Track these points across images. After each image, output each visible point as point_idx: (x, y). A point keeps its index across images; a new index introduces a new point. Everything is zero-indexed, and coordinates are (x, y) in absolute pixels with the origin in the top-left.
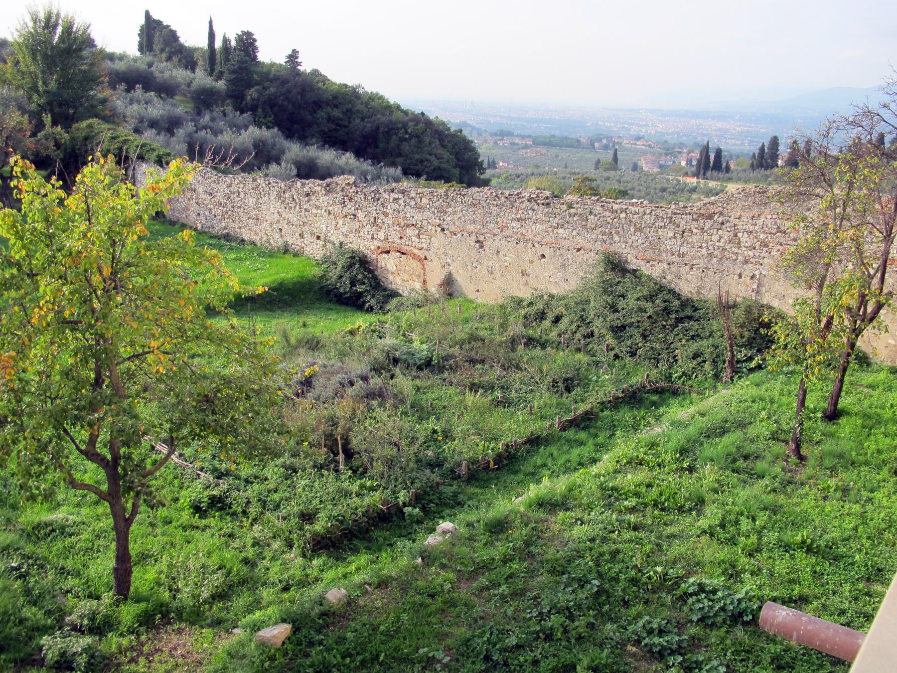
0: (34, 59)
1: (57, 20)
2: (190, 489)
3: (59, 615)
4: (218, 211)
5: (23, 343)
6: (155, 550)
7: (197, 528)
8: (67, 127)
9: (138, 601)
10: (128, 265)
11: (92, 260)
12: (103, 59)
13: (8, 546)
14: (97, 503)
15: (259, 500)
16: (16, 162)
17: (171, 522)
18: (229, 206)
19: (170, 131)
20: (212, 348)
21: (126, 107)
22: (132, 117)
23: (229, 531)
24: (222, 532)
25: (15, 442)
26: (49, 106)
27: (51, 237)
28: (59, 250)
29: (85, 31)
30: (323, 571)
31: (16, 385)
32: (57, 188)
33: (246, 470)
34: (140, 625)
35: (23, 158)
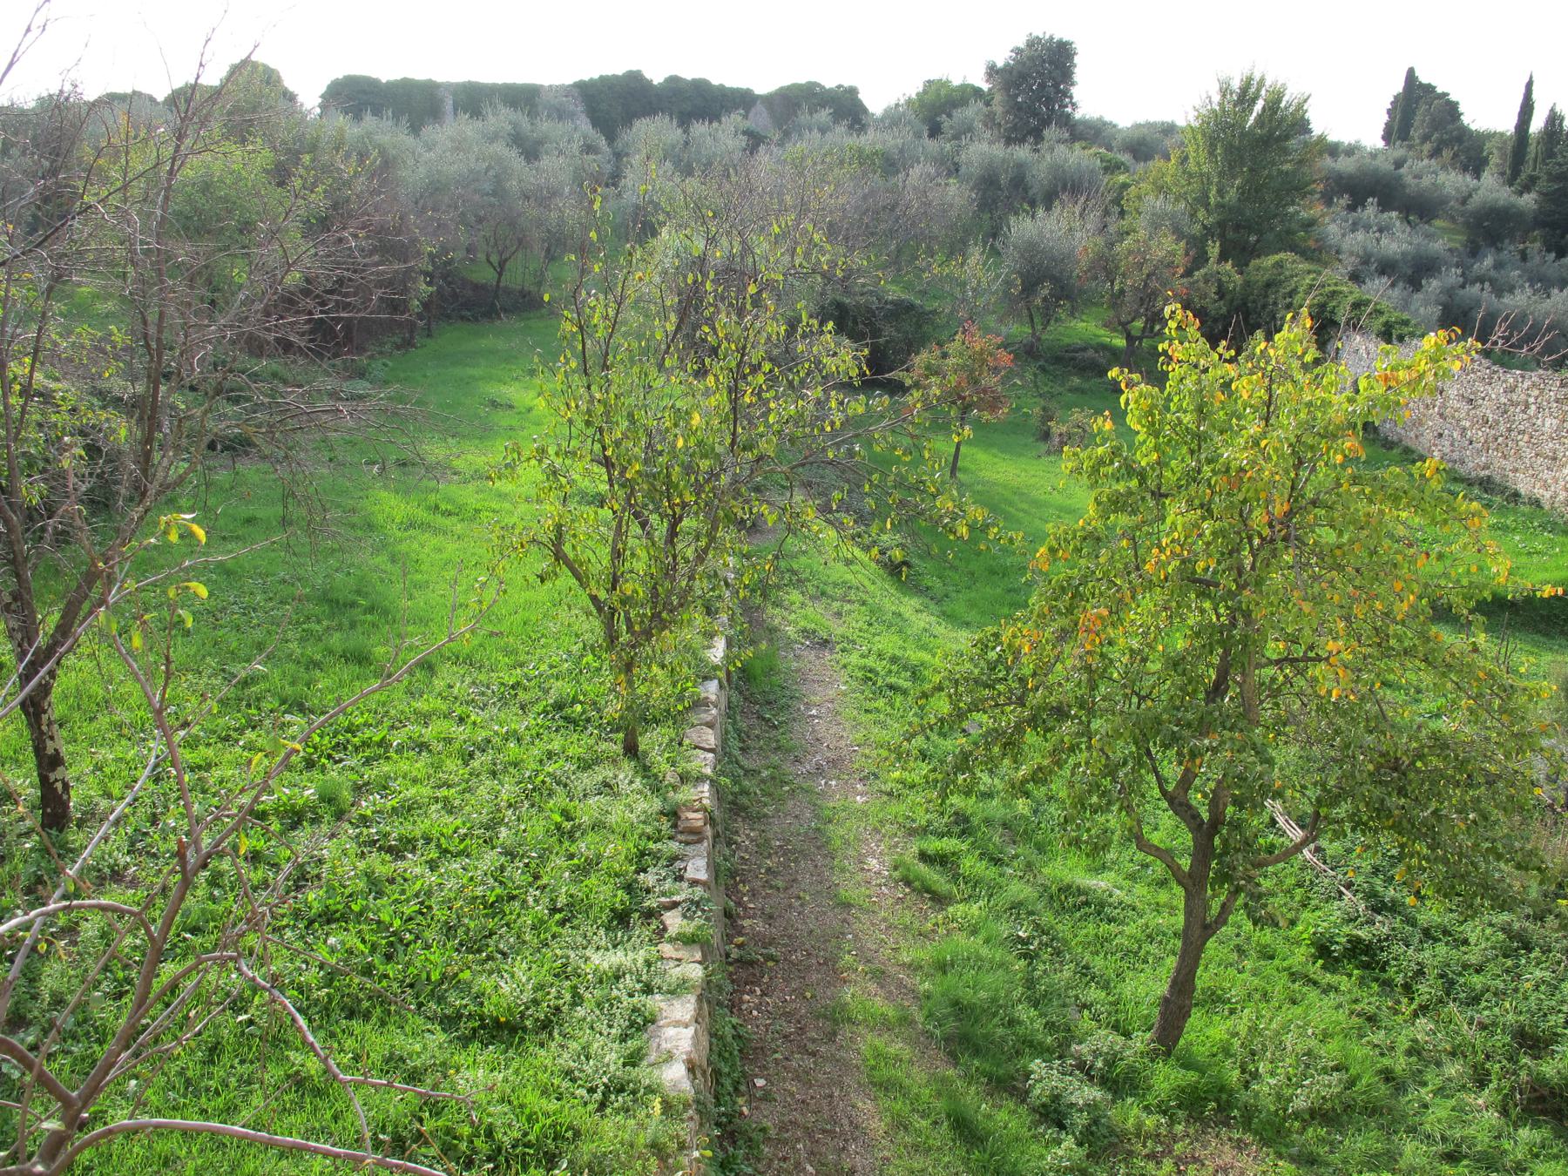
0: (1212, 153)
1: (1258, 90)
2: (1318, 913)
3: (1066, 1036)
4: (1480, 435)
5: (1121, 600)
6: (1235, 993)
7: (1315, 983)
8: (1241, 266)
9: (1187, 1064)
10: (1314, 503)
11: (1260, 485)
12: (1321, 153)
13: (1021, 903)
14: (1162, 883)
15: (1442, 976)
16: (1173, 312)
17: (1272, 958)
18: (1502, 428)
19: (1415, 283)
20: (1428, 678)
21: (1344, 235)
22: (1352, 254)
23: (1372, 1009)
24: (1358, 1007)
25: (1072, 749)
26: (1219, 230)
27: (1201, 438)
28: (1209, 461)
29: (1300, 106)
30: (1537, 1156)
31: (1095, 662)
32: (1225, 361)
33: (1432, 913)
34: (1179, 1107)
35: (1185, 308)
